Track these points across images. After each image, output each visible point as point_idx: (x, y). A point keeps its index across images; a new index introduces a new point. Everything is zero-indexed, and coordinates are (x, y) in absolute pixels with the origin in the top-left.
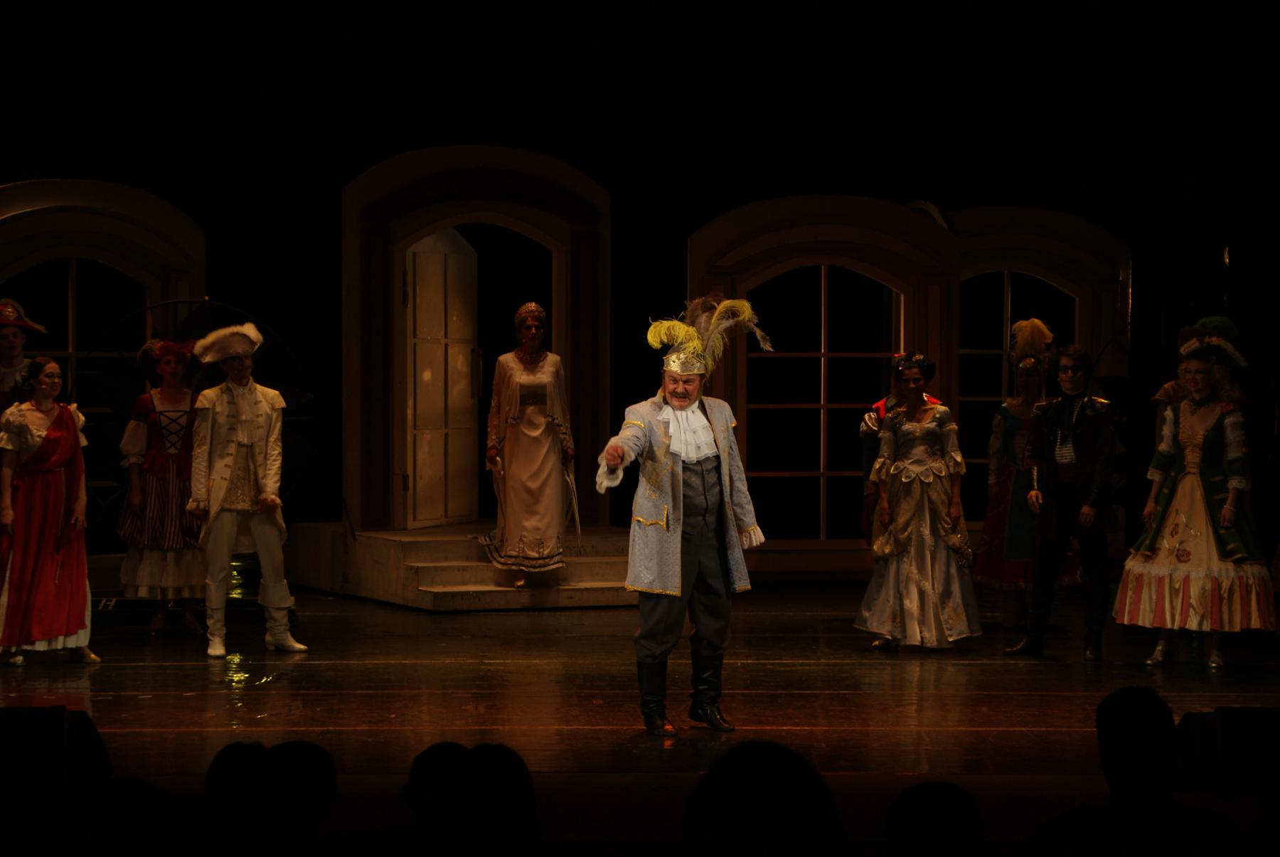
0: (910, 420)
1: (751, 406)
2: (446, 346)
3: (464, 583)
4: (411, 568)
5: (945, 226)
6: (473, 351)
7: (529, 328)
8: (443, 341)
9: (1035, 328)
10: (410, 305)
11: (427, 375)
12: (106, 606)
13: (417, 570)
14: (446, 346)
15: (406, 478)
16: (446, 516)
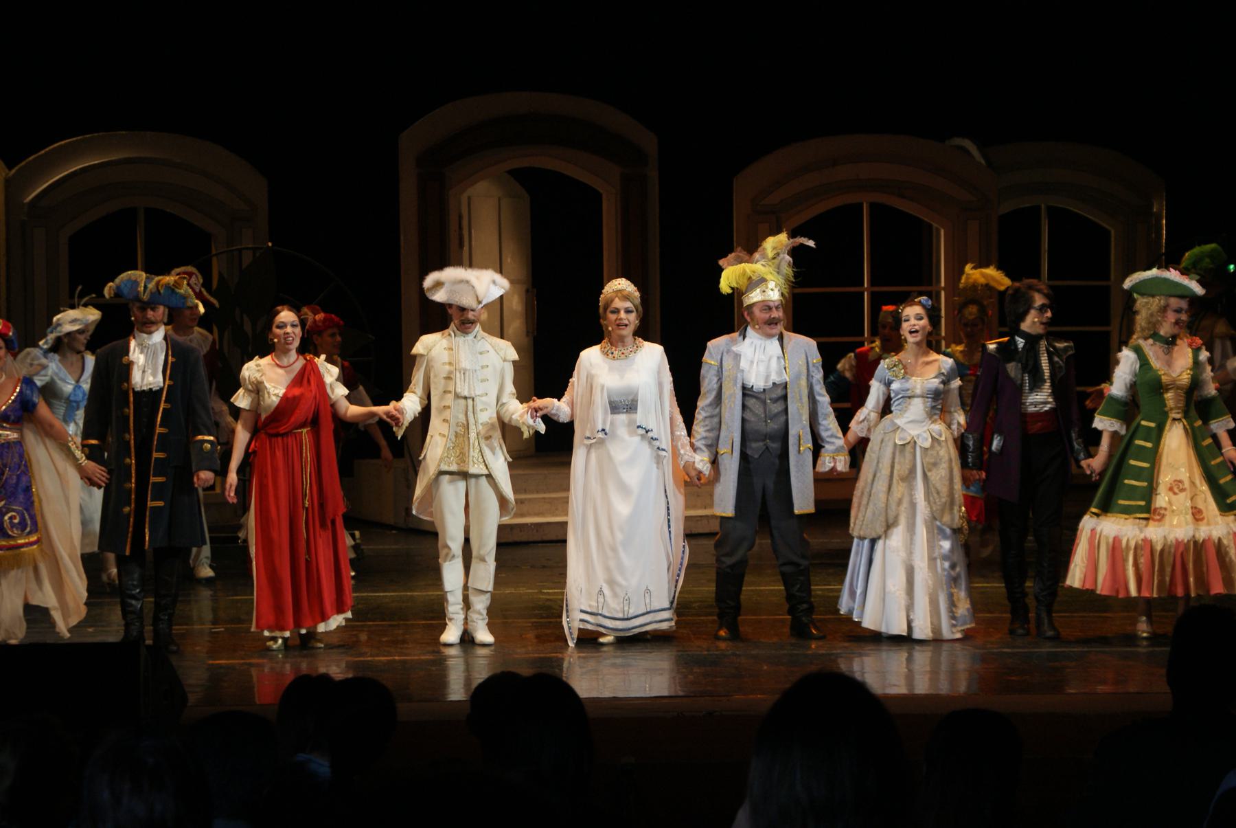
5: (983, 162)
6: (527, 291)
10: (466, 248)
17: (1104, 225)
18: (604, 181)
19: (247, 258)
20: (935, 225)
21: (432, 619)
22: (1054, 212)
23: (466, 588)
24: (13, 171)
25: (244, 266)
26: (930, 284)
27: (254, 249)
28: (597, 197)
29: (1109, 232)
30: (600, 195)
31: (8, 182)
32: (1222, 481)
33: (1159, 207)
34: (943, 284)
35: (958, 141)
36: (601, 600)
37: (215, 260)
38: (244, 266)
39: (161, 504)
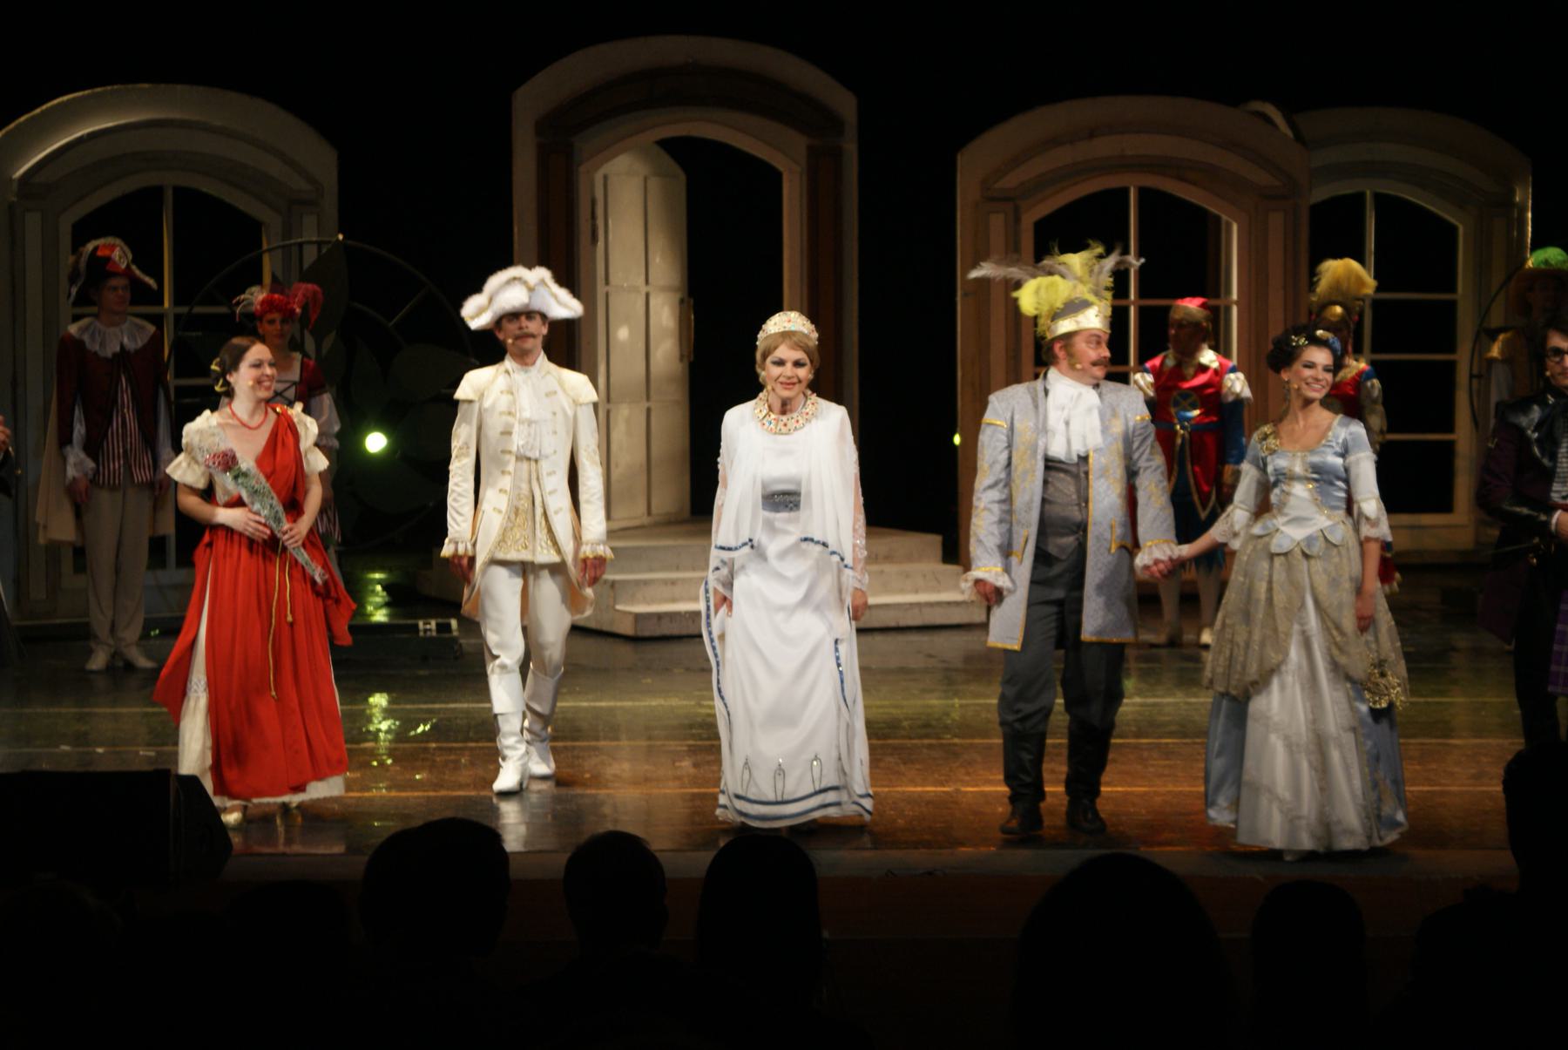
5: (1290, 133)
6: (682, 301)
10: (601, 244)
19: (310, 255)
28: (777, 176)
33: (1523, 196)
35: (1257, 106)
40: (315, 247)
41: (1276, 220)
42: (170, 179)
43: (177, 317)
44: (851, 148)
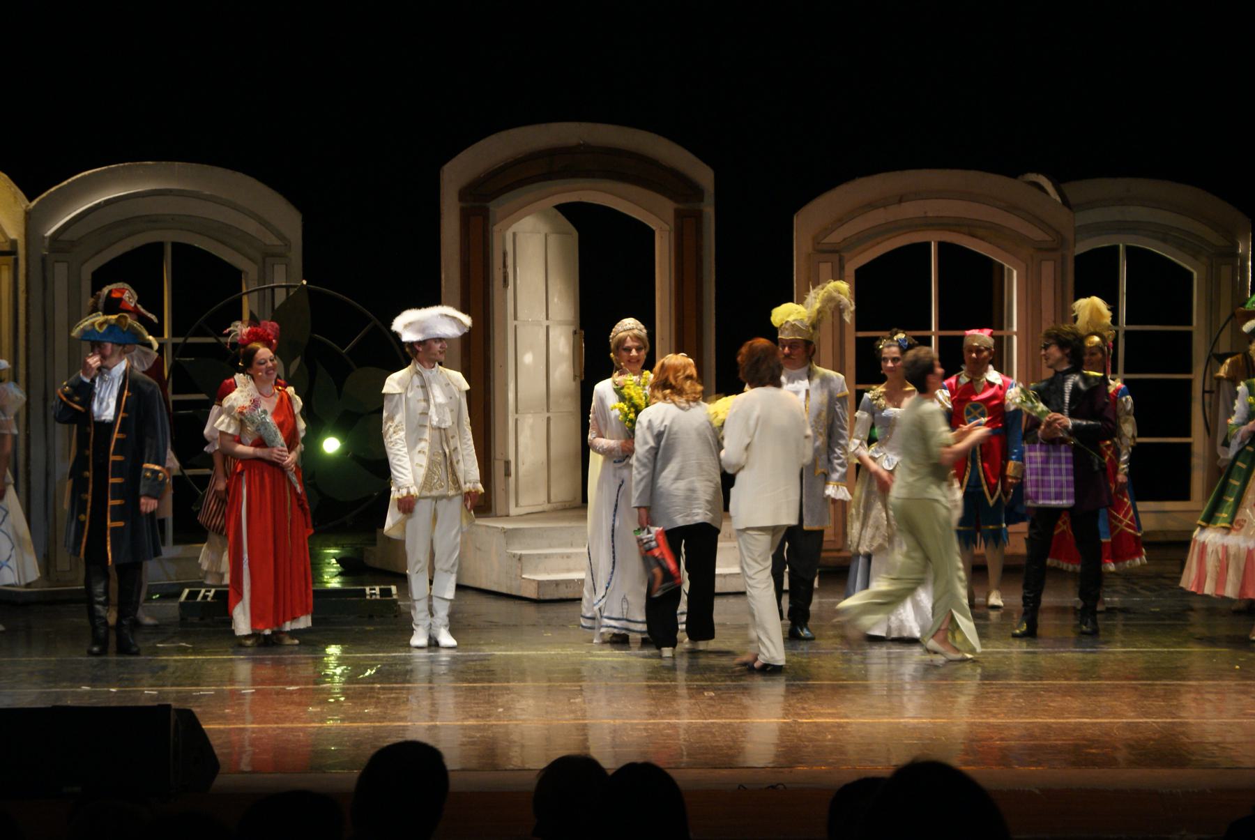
0: (1103, 457)
1: (861, 334)
2: (548, 328)
3: (569, 570)
4: (514, 556)
5: (1059, 199)
6: (575, 333)
7: (629, 350)
8: (545, 323)
9: (1095, 311)
10: (511, 287)
11: (527, 359)
12: (205, 597)
13: (520, 558)
14: (548, 328)
15: (507, 463)
16: (549, 501)
17: (1188, 268)
18: (653, 213)
19: (280, 297)
20: (1006, 266)
21: (475, 681)
22: (1132, 252)
23: (430, 598)
24: (34, 203)
25: (277, 306)
26: (1001, 328)
27: (288, 287)
28: (651, 233)
29: (1190, 274)
30: (652, 233)
31: (28, 215)
32: (1103, 540)
34: (1015, 329)
36: (625, 606)
37: (245, 299)
38: (277, 306)
39: (121, 524)
40: (284, 290)
41: (1048, 269)
42: (168, 237)
43: (175, 346)
44: (709, 211)
